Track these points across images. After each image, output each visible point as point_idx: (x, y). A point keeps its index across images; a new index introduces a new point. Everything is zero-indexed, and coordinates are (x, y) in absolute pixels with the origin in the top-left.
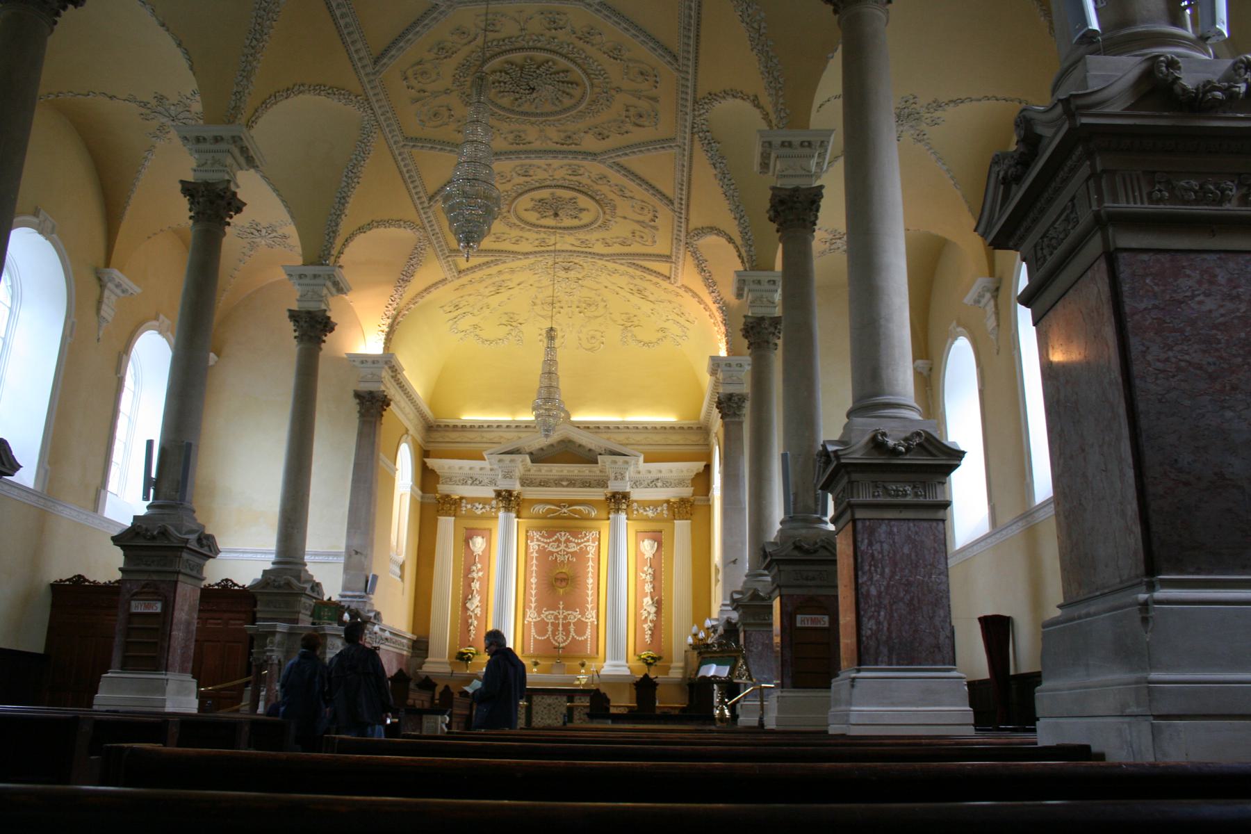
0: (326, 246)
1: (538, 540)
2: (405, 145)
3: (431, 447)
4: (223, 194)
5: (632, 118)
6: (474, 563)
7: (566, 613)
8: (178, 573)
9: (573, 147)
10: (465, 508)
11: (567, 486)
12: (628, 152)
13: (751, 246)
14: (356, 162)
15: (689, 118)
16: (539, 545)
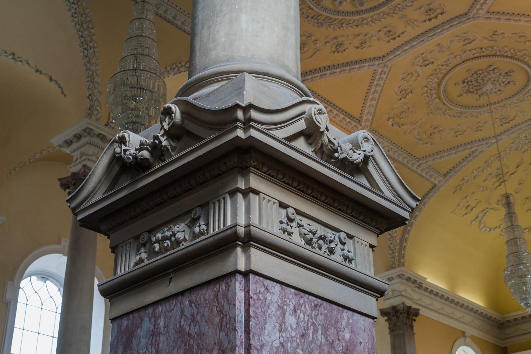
9: (441, 19)
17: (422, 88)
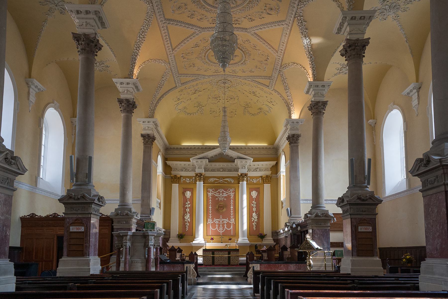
0: (131, 70)
1: (211, 192)
2: (165, 22)
3: (168, 156)
4: (93, 40)
5: (267, 11)
6: (187, 202)
7: (223, 220)
8: (91, 214)
10: (182, 180)
11: (222, 171)
12: (262, 28)
13: (314, 70)
14: (143, 30)
15: (295, 9)
16: (212, 194)
17: (203, 47)
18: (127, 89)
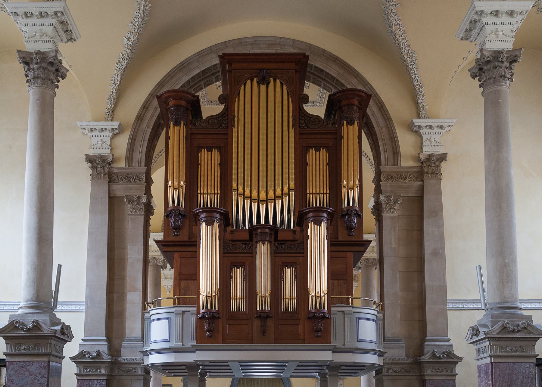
18: (102, 140)
